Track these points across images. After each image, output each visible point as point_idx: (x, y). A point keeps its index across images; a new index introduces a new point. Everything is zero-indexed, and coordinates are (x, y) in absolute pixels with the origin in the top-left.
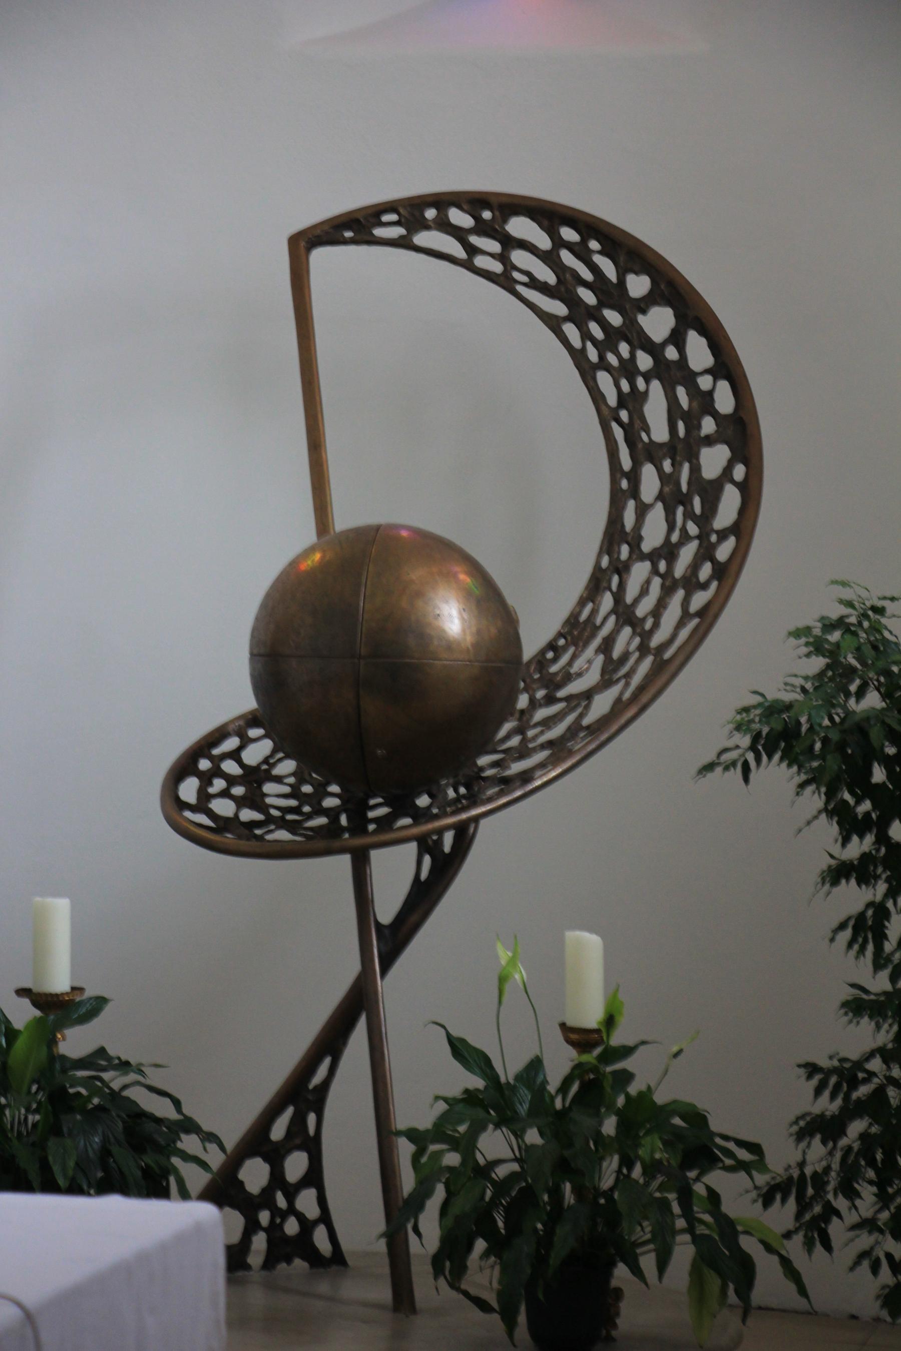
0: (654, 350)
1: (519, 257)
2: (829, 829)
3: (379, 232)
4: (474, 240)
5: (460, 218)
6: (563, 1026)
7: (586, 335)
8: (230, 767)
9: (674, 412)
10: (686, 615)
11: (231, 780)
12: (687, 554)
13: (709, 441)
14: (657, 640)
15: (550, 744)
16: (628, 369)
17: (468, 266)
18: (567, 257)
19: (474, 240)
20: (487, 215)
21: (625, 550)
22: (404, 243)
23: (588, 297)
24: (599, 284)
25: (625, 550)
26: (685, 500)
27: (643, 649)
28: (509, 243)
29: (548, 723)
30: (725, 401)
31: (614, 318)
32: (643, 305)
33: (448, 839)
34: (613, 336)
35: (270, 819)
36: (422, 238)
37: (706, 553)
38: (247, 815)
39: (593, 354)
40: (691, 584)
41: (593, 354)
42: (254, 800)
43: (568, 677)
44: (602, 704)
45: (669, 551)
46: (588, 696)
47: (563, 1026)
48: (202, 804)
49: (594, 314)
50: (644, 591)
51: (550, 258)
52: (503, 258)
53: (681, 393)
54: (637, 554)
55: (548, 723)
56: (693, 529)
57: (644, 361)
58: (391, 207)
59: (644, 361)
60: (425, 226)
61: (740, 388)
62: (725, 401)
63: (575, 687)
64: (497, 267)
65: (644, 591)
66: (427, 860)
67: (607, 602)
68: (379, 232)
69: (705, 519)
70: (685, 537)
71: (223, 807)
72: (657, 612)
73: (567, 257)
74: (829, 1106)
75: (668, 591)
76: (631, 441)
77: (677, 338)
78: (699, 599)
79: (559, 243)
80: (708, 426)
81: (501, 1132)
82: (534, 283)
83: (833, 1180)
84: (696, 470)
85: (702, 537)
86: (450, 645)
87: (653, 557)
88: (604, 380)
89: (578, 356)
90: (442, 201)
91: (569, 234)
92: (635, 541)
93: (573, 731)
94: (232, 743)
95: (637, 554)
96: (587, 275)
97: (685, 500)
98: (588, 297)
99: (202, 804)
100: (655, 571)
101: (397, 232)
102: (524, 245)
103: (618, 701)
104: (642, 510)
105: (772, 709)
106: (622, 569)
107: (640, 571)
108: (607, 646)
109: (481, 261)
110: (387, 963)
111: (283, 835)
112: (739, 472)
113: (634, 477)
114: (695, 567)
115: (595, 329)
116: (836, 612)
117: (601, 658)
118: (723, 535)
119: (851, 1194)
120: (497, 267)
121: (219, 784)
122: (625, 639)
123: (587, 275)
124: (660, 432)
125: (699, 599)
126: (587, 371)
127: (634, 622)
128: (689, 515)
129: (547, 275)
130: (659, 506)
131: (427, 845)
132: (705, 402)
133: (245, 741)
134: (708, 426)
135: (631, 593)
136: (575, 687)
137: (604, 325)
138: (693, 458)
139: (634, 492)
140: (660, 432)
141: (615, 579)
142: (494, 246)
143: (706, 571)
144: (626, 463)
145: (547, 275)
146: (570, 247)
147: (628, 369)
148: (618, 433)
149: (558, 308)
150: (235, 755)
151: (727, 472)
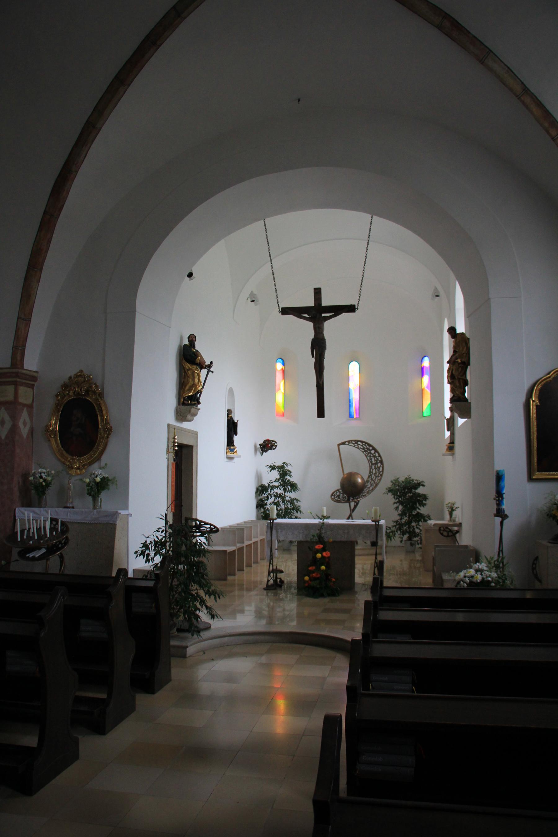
0: (373, 454)
1: (359, 446)
2: (393, 499)
3: (346, 444)
4: (355, 444)
5: (353, 442)
6: (192, 339)
7: (366, 453)
8: (336, 495)
9: (375, 460)
10: (378, 480)
11: (336, 496)
12: (377, 474)
13: (379, 463)
14: (376, 482)
15: (367, 492)
16: (370, 456)
17: (354, 447)
18: (364, 446)
19: (355, 444)
20: (356, 442)
21: (371, 474)
22: (348, 445)
23: (366, 449)
24: (367, 448)
25: (371, 474)
26: (377, 469)
27: (374, 483)
28: (358, 444)
29: (366, 490)
30: (380, 459)
31: (369, 451)
32: (371, 450)
33: (357, 502)
34: (369, 453)
35: (341, 500)
36: (350, 444)
37: (379, 473)
38: (339, 499)
39: (367, 455)
40: (378, 476)
41: (367, 455)
42: (339, 498)
43: (367, 486)
44: (371, 488)
45: (376, 474)
46: (370, 487)
47: (192, 339)
48: (334, 498)
49: (367, 451)
50: (374, 477)
51: (362, 446)
52: (358, 446)
53: (375, 458)
54: (373, 474)
55: (366, 490)
56: (378, 471)
57: (372, 455)
58: (347, 441)
59: (372, 455)
60: (350, 443)
61: (381, 458)
62: (380, 459)
63: (368, 487)
64: (357, 447)
65: (374, 477)
66: (355, 503)
67: (370, 478)
68: (346, 444)
69: (379, 470)
70: (377, 472)
71: (337, 499)
72: (375, 479)
73: (364, 446)
74: (395, 524)
75: (376, 477)
76: (371, 463)
77: (375, 453)
78: (379, 478)
79: (363, 444)
80: (378, 461)
81: (348, 506)
82: (361, 448)
83: (396, 531)
84: (377, 466)
85: (379, 472)
86: (360, 483)
87: (374, 474)
88: (368, 457)
89: (365, 455)
90: (352, 441)
91: (364, 444)
92: (372, 472)
93: (369, 491)
94: (335, 493)
95: (373, 474)
96: (366, 447)
97: (377, 469)
98: (366, 449)
99: (334, 498)
100: (374, 475)
101: (348, 444)
102: (360, 445)
103: (373, 488)
104: (373, 470)
105: (390, 488)
106: (371, 475)
107: (373, 475)
108: (371, 483)
109: (356, 446)
110: (353, 512)
111: (343, 501)
112: (382, 466)
113: (372, 466)
114: (378, 475)
115: (367, 452)
116: (394, 479)
117: (370, 484)
118: (381, 472)
119: (397, 532)
120: (357, 447)
121: (335, 497)
122: (372, 482)
123: (366, 447)
124: (374, 462)
125: (379, 478)
126: (366, 456)
127: (373, 480)
128: (377, 470)
129: (362, 447)
130: (374, 469)
131: (355, 502)
132: (378, 459)
133: (337, 493)
134: (378, 461)
135: (372, 478)
136: (368, 487)
137: (368, 452)
138: (377, 464)
139: (372, 468)
140: (374, 462)
141: (371, 476)
142: (357, 445)
143: (379, 475)
144: (371, 465)
145: (362, 447)
146: (364, 445)
147: (370, 456)
148: (370, 462)
149: (363, 450)
150: (336, 494)
151: (380, 466)
